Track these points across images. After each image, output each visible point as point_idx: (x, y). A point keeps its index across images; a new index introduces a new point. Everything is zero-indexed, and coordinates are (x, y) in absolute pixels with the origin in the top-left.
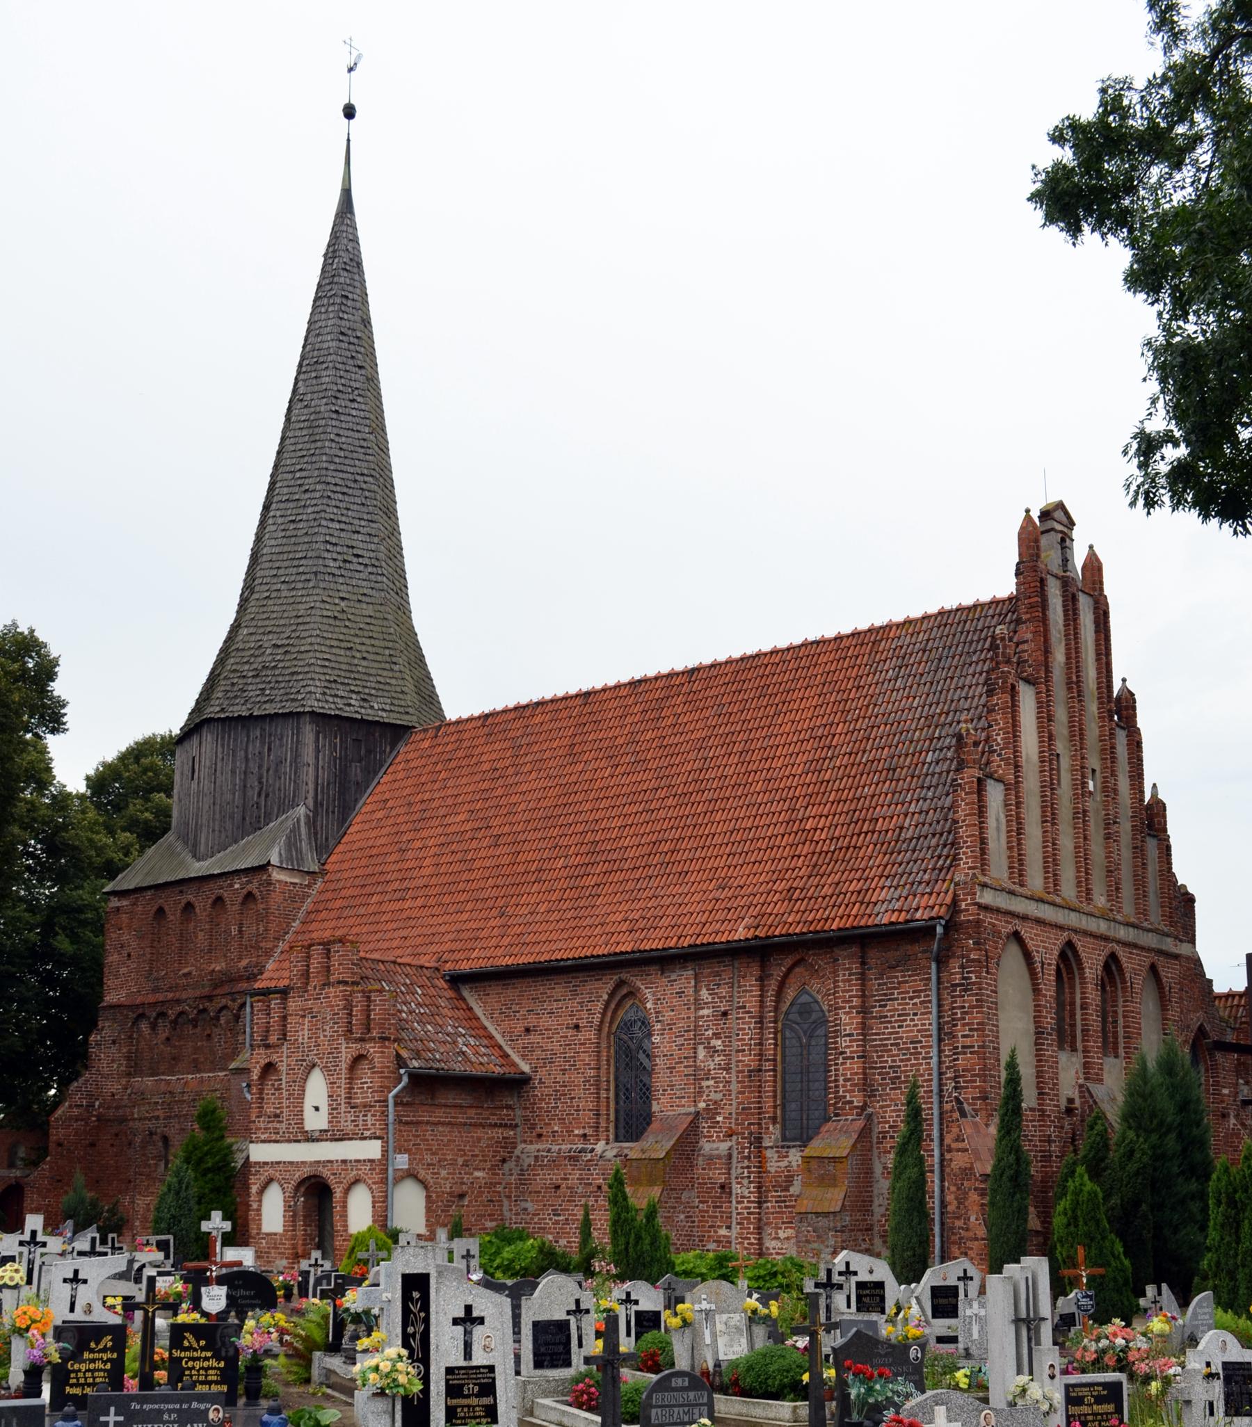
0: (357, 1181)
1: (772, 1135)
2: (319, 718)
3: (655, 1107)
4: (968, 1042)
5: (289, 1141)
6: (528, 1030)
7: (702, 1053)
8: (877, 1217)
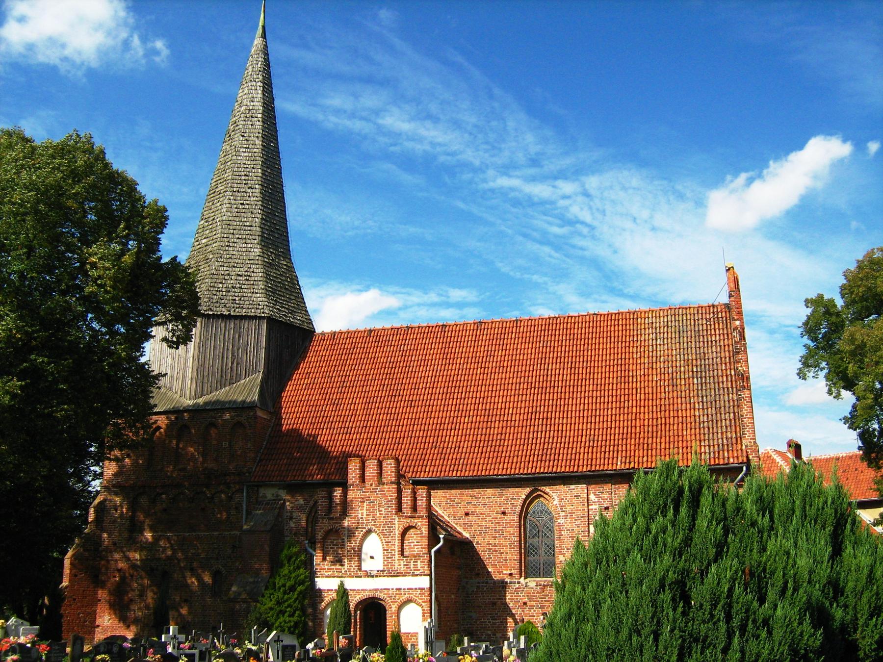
0: (409, 601)
6: (467, 514)
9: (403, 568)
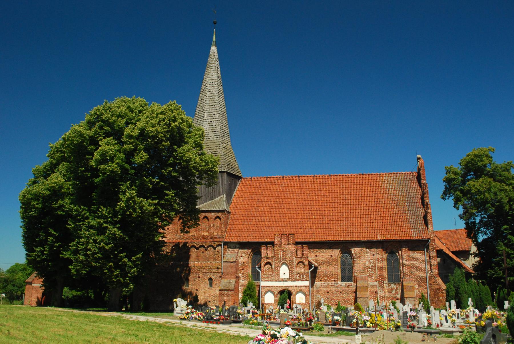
1: (386, 281)
2: (227, 172)
3: (355, 274)
6: (316, 256)
7: (367, 263)
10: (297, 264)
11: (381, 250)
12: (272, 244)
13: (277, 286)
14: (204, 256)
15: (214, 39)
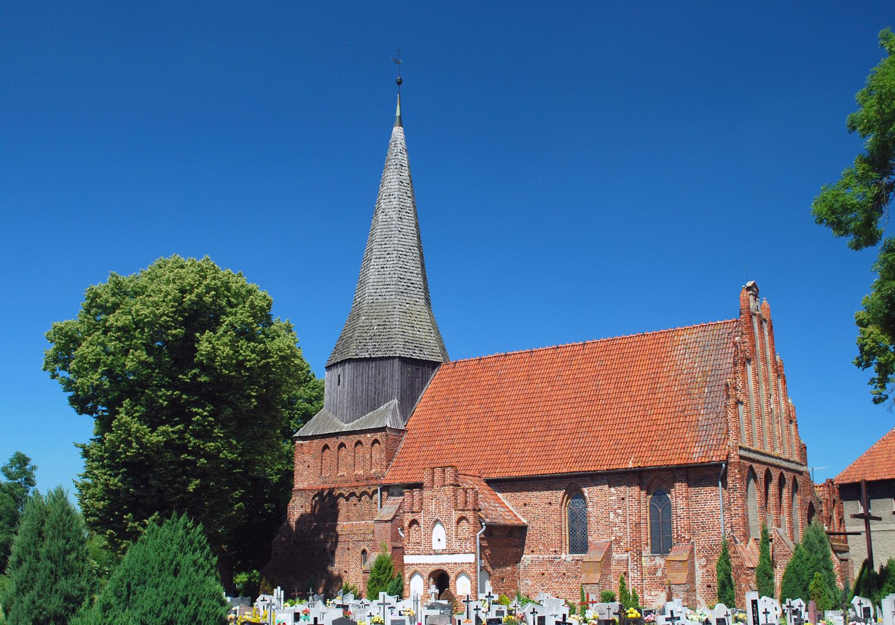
1: (647, 551)
2: (403, 359)
3: (590, 539)
4: (737, 512)
5: (425, 554)
6: (525, 505)
7: (612, 515)
8: (697, 585)
9: (458, 548)
10: (458, 522)
11: (637, 489)
12: (420, 486)
13: (427, 564)
14: (357, 512)
15: (398, 114)
